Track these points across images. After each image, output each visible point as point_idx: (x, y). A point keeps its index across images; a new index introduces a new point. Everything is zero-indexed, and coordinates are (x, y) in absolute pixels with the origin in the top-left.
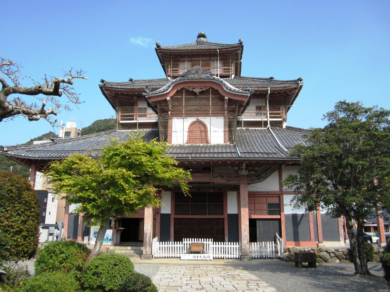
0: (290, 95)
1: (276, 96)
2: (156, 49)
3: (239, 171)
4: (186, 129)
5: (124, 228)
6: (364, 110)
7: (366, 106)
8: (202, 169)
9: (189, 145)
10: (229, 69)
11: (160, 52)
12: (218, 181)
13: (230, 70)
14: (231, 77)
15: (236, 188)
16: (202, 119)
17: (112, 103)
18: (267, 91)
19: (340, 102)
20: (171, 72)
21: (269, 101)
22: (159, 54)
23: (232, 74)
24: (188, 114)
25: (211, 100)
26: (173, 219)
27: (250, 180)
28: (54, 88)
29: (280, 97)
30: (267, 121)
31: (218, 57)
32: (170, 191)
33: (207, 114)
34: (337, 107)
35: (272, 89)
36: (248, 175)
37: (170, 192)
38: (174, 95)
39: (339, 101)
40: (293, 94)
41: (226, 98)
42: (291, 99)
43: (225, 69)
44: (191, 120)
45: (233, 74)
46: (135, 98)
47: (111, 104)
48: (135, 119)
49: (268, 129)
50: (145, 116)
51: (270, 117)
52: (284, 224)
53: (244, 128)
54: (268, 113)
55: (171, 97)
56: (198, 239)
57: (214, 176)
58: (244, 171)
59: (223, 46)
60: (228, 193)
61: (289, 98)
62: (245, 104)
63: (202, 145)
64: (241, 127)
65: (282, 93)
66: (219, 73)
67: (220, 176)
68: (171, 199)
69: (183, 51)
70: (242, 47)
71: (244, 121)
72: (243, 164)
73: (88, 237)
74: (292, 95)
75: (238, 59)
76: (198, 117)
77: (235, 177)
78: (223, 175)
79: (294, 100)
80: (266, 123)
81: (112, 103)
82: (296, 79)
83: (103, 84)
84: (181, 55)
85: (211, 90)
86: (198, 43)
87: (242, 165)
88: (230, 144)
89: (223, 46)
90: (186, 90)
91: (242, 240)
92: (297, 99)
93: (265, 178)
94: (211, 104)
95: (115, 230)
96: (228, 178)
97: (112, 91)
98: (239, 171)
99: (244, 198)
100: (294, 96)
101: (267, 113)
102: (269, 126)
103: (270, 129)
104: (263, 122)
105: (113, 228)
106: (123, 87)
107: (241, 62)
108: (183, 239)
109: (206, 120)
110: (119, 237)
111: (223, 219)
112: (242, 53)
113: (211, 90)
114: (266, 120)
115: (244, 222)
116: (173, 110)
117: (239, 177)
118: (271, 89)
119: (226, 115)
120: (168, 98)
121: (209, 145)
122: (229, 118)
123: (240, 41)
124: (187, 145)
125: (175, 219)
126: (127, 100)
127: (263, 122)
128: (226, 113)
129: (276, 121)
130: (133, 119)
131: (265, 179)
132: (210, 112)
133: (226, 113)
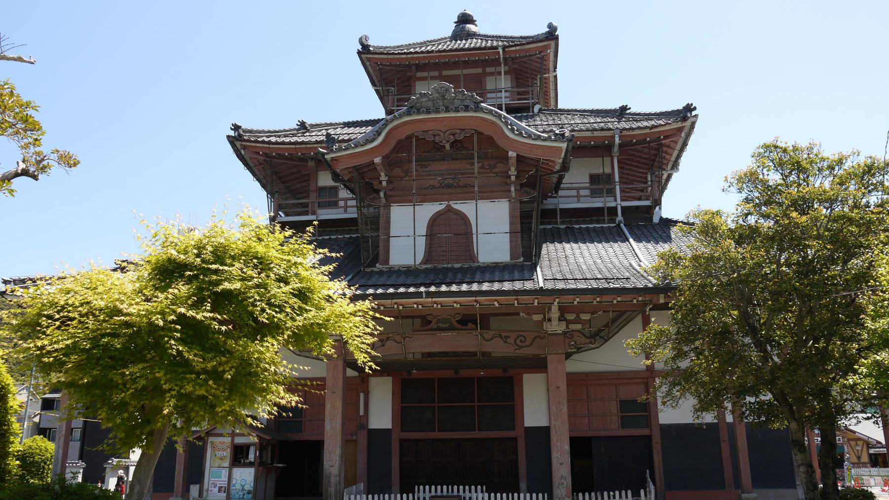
0: (668, 146)
1: (635, 150)
2: (359, 53)
3: (544, 323)
4: (422, 229)
5: (285, 465)
6: (825, 164)
7: (830, 152)
8: (458, 322)
9: (429, 266)
10: (527, 93)
11: (369, 60)
12: (498, 348)
13: (530, 96)
14: (533, 112)
15: (539, 365)
16: (458, 206)
17: (261, 177)
18: (613, 137)
19: (766, 147)
20: (396, 103)
21: (619, 162)
22: (368, 63)
23: (534, 104)
24: (425, 197)
25: (476, 160)
26: (398, 441)
27: (570, 346)
28: (611, 288)
29: (646, 150)
30: (615, 208)
31: (501, 66)
32: (388, 375)
33: (468, 193)
34: (758, 156)
35: (625, 133)
36: (564, 333)
37: (390, 379)
38: (391, 152)
39: (762, 144)
40: (676, 143)
41: (512, 154)
42: (671, 155)
43: (519, 93)
44: (428, 210)
45: (537, 103)
46: (311, 164)
47: (259, 180)
48: (310, 212)
49: (619, 225)
50: (334, 204)
51: (622, 200)
52: (660, 448)
53: (563, 227)
54: (618, 188)
55: (385, 158)
56: (450, 487)
57: (486, 336)
58: (555, 322)
59: (512, 42)
60: (526, 377)
61: (666, 152)
62: (557, 167)
63: (457, 266)
64: (556, 223)
65: (649, 142)
66: (504, 103)
67: (501, 337)
68: (393, 394)
69: (421, 55)
70: (556, 38)
71: (561, 210)
72: (553, 307)
73: (198, 486)
74: (672, 144)
75: (548, 69)
76: (448, 201)
77: (535, 338)
78: (507, 334)
79: (679, 156)
80: (613, 211)
81: (261, 177)
82: (680, 107)
83: (236, 134)
84: (417, 66)
85: (475, 137)
86: (456, 36)
87: (550, 309)
88: (524, 261)
89: (512, 42)
90: (417, 139)
91: (555, 487)
92: (685, 155)
93: (606, 338)
94: (476, 171)
95: (261, 468)
96: (518, 342)
97: (257, 150)
98: (544, 323)
99: (558, 387)
100: (678, 147)
101: (615, 188)
102: (620, 217)
103: (622, 225)
104: (606, 210)
105: (256, 465)
106: (282, 139)
107: (556, 77)
108: (416, 488)
109: (466, 208)
110: (271, 485)
111: (515, 439)
112: (556, 56)
113: (475, 137)
114: (613, 204)
115: (559, 444)
116: (391, 186)
117: (545, 337)
118: (621, 132)
119: (513, 195)
120: (377, 160)
121: (476, 264)
122: (522, 202)
123: (550, 26)
124: (424, 266)
125: (402, 442)
126: (294, 170)
127: (606, 210)
128: (513, 189)
129: (637, 207)
130: (306, 213)
131: (606, 341)
132: (476, 189)
133: (513, 189)
